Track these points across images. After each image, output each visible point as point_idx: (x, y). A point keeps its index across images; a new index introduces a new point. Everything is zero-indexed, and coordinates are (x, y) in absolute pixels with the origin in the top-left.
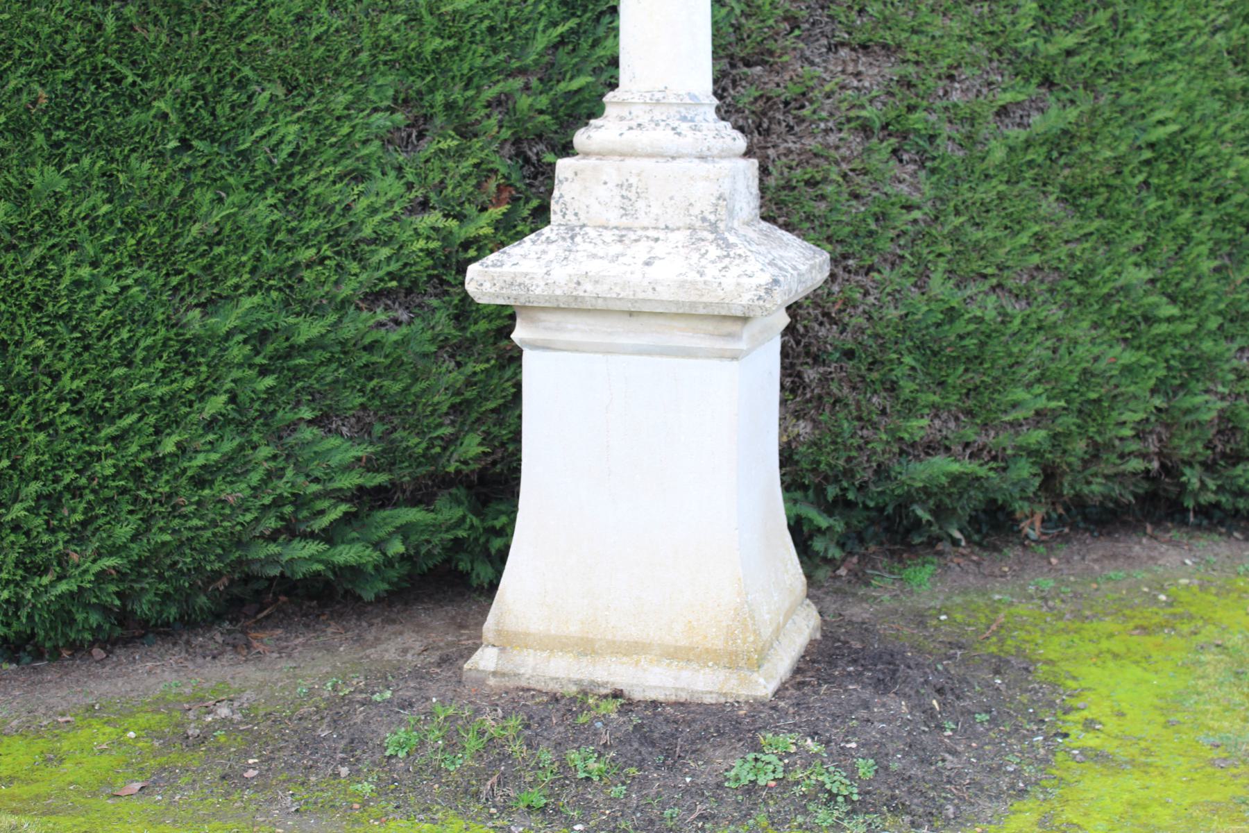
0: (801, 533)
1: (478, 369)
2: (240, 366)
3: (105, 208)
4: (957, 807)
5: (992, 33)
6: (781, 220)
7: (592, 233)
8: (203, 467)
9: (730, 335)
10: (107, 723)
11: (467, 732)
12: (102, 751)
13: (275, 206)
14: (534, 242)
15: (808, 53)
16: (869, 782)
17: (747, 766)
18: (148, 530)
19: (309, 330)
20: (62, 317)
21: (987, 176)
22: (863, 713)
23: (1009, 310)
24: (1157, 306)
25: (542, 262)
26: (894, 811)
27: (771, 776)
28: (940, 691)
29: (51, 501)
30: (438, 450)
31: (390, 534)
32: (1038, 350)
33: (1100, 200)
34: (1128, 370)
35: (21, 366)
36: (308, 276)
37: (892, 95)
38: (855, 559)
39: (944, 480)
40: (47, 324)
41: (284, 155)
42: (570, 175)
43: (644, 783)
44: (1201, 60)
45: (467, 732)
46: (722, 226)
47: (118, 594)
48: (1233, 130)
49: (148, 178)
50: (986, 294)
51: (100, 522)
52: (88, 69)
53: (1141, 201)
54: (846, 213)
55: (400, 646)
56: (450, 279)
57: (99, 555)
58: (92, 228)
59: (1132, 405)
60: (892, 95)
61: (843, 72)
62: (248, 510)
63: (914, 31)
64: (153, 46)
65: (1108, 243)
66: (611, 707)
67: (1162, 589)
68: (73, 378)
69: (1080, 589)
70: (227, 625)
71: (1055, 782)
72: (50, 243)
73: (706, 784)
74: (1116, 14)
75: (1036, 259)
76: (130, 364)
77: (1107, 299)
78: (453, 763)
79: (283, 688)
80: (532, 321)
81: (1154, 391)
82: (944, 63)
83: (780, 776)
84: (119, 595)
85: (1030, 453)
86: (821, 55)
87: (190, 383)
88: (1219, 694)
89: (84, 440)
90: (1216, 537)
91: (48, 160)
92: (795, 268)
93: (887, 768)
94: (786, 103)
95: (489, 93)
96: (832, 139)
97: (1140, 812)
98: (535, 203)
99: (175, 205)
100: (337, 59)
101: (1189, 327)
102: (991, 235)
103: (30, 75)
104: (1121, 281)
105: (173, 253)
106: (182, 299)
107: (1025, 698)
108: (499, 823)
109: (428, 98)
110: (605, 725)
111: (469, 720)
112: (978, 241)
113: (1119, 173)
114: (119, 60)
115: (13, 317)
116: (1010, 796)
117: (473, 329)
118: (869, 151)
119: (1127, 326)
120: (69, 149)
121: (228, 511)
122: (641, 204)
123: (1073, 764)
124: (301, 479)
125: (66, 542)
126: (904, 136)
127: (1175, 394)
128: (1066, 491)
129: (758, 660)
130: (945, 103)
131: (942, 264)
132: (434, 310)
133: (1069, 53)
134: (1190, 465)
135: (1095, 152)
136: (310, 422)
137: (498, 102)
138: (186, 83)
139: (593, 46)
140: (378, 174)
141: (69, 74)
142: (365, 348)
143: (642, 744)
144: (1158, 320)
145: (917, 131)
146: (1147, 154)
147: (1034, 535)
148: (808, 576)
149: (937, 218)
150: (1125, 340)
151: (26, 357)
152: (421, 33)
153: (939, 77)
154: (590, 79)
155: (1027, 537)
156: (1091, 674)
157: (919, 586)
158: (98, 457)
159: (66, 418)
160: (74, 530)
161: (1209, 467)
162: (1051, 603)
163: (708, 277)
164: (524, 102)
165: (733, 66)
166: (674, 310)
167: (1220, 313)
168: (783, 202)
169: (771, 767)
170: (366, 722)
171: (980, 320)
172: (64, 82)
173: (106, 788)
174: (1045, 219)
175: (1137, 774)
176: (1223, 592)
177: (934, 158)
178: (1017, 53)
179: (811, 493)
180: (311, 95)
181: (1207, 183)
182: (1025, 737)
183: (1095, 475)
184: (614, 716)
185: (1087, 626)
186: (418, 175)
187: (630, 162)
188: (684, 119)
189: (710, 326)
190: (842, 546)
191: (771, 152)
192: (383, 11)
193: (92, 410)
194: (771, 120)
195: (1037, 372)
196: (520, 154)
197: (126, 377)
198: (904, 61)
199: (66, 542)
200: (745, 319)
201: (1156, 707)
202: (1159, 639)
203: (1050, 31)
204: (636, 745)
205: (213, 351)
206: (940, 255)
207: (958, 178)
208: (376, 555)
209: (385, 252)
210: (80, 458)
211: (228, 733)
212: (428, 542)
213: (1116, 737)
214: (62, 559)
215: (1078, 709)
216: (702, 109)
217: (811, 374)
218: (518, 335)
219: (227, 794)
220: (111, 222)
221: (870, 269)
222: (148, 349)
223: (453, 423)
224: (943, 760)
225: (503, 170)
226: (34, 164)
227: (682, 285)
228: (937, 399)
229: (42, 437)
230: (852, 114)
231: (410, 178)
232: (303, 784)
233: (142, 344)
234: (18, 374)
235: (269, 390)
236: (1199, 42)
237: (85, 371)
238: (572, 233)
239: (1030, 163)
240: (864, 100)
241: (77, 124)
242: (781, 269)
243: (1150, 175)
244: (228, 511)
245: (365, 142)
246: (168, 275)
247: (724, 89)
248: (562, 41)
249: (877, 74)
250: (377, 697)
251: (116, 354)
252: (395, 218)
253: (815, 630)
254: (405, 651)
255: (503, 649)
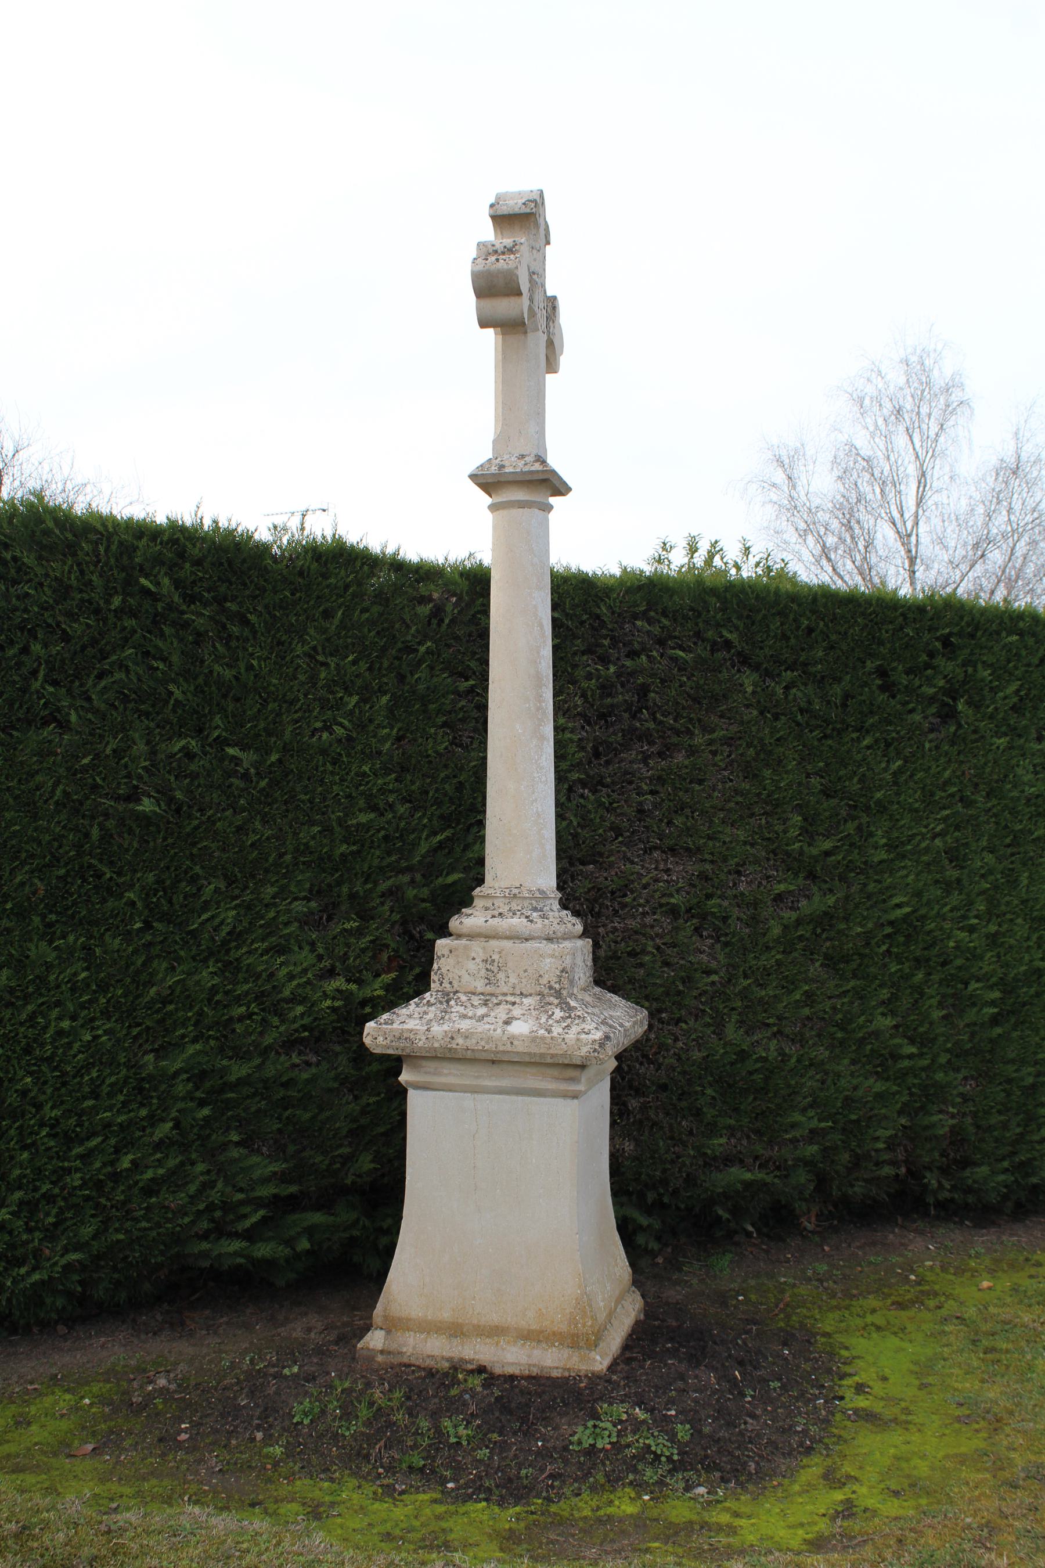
0: (626, 1230)
1: (371, 1101)
2: (183, 1099)
3: (84, 975)
4: (757, 1463)
5: (769, 839)
6: (609, 983)
7: (463, 998)
8: (152, 1179)
9: (572, 1080)
10: (68, 1391)
11: (360, 1402)
12: (62, 1416)
13: (215, 973)
14: (417, 1005)
15: (629, 854)
16: (687, 1444)
17: (588, 1432)
18: (106, 1230)
19: (239, 1071)
20: (47, 1059)
21: (767, 948)
22: (680, 1384)
23: (787, 1051)
24: (901, 1046)
25: (424, 1021)
26: (708, 1469)
27: (607, 1440)
28: (741, 1363)
29: (29, 1207)
30: (338, 1166)
31: (299, 1234)
32: (810, 1082)
33: (854, 965)
34: (880, 1096)
35: (12, 1099)
36: (239, 1028)
37: (694, 886)
38: (669, 1250)
39: (739, 1186)
40: (35, 1065)
41: (223, 934)
42: (446, 952)
43: (503, 1446)
44: (925, 858)
45: (360, 1402)
46: (564, 993)
47: (80, 1282)
48: (951, 911)
49: (118, 951)
50: (769, 1039)
51: (68, 1223)
52: (77, 868)
53: (885, 965)
54: (659, 977)
55: (305, 1327)
56: (351, 1030)
57: (66, 1250)
58: (73, 990)
59: (883, 1124)
60: (694, 886)
61: (656, 869)
62: (186, 1214)
63: (710, 838)
64: (127, 850)
65: (861, 998)
66: (476, 1382)
67: (913, 1271)
68: (52, 1108)
69: (847, 1271)
70: (165, 1306)
71: (834, 1439)
72: (40, 1001)
73: (554, 1448)
74: (861, 824)
75: (806, 1011)
76: (96, 1098)
77: (862, 1042)
78: (348, 1429)
79: (210, 1362)
80: (416, 1067)
81: (900, 1113)
82: (733, 862)
83: (614, 1440)
84: (81, 1283)
85: (806, 1163)
86: (639, 856)
87: (144, 1112)
88: (960, 1359)
89: (59, 1158)
90: (952, 1226)
91: (42, 938)
92: (621, 1025)
93: (700, 1432)
94: (613, 893)
95: (383, 886)
96: (648, 920)
97: (904, 1465)
98: (417, 970)
99: (138, 972)
100: (267, 860)
101: (926, 1062)
102: (771, 993)
103: (32, 872)
104: (872, 1028)
105: (135, 1010)
106: (141, 1046)
107: (807, 1366)
108: (386, 1481)
109: (336, 890)
110: (472, 1397)
111: (362, 1392)
112: (762, 998)
113: (868, 944)
114: (101, 861)
115: (8, 1059)
116: (800, 1453)
117: (368, 1069)
118: (676, 929)
119: (878, 1062)
120: (59, 929)
121: (170, 1215)
122: (501, 976)
123: (849, 1423)
124: (229, 1189)
125: (40, 1240)
126: (703, 917)
127: (916, 1114)
128: (835, 1192)
129: (594, 1341)
130: (734, 892)
131: (735, 1017)
132: (337, 1054)
133: (827, 854)
134: (930, 1170)
135: (849, 928)
136: (238, 1144)
137: (390, 893)
138: (151, 877)
139: (464, 850)
140: (296, 949)
141: (62, 872)
142: (282, 1085)
143: (501, 1413)
144: (902, 1057)
145: (713, 913)
146: (889, 930)
147: (810, 1227)
148: (632, 1265)
149: (730, 980)
150: (877, 1073)
151: (16, 1091)
152: (332, 841)
153: (729, 872)
154: (461, 875)
155: (805, 1229)
156: (859, 1344)
157: (721, 1271)
158: (69, 1171)
159: (46, 1140)
160: (47, 1230)
161: (944, 1171)
162: (825, 1284)
163: (555, 1034)
164: (411, 893)
165: (572, 864)
166: (527, 1059)
167: (948, 1051)
168: (611, 969)
169: (607, 1433)
170: (277, 1393)
171: (765, 1060)
172: (58, 878)
173: (63, 1448)
174: (813, 981)
175: (900, 1431)
176: (959, 1272)
177: (726, 935)
178: (788, 854)
179: (634, 1197)
180: (246, 887)
181: (935, 951)
182: (809, 1400)
183: (857, 1179)
184: (479, 1389)
185: (854, 1303)
186: (327, 949)
187: (494, 943)
188: (535, 909)
189: (555, 1072)
190: (658, 1239)
191: (601, 930)
192: (303, 824)
193: (66, 1134)
194: (601, 905)
195: (810, 1099)
196: (407, 932)
197: (94, 1107)
198: (702, 861)
199: (40, 1240)
200: (583, 1067)
201: (912, 1372)
202: (911, 1313)
203: (812, 837)
204: (497, 1414)
205: (163, 1087)
206: (733, 1009)
207: (745, 949)
208: (287, 1251)
209: (300, 1009)
210: (54, 1172)
211: (165, 1402)
212: (329, 1239)
213: (882, 1399)
214: (37, 1253)
215: (851, 1375)
216: (549, 902)
217: (634, 1103)
218: (404, 1077)
219: (163, 1455)
220: (88, 986)
221: (679, 1020)
222: (111, 1085)
223: (350, 1144)
224: (745, 1423)
225: (393, 945)
226: (31, 940)
227: (534, 1040)
228: (732, 1122)
229: (25, 1155)
230: (663, 901)
231: (321, 951)
232: (225, 1447)
233: (108, 1082)
234: (10, 1105)
235: (206, 1119)
236: (924, 845)
237: (62, 1103)
238: (447, 997)
239: (801, 938)
240: (672, 889)
241: (67, 909)
242: (611, 1026)
243: (891, 946)
244: (170, 1215)
245: (287, 924)
246: (130, 1027)
247: (565, 882)
248: (441, 845)
249: (681, 870)
250: (286, 1371)
251: (87, 1089)
252: (308, 982)
253: (639, 1312)
254: (309, 1330)
255: (389, 1332)
